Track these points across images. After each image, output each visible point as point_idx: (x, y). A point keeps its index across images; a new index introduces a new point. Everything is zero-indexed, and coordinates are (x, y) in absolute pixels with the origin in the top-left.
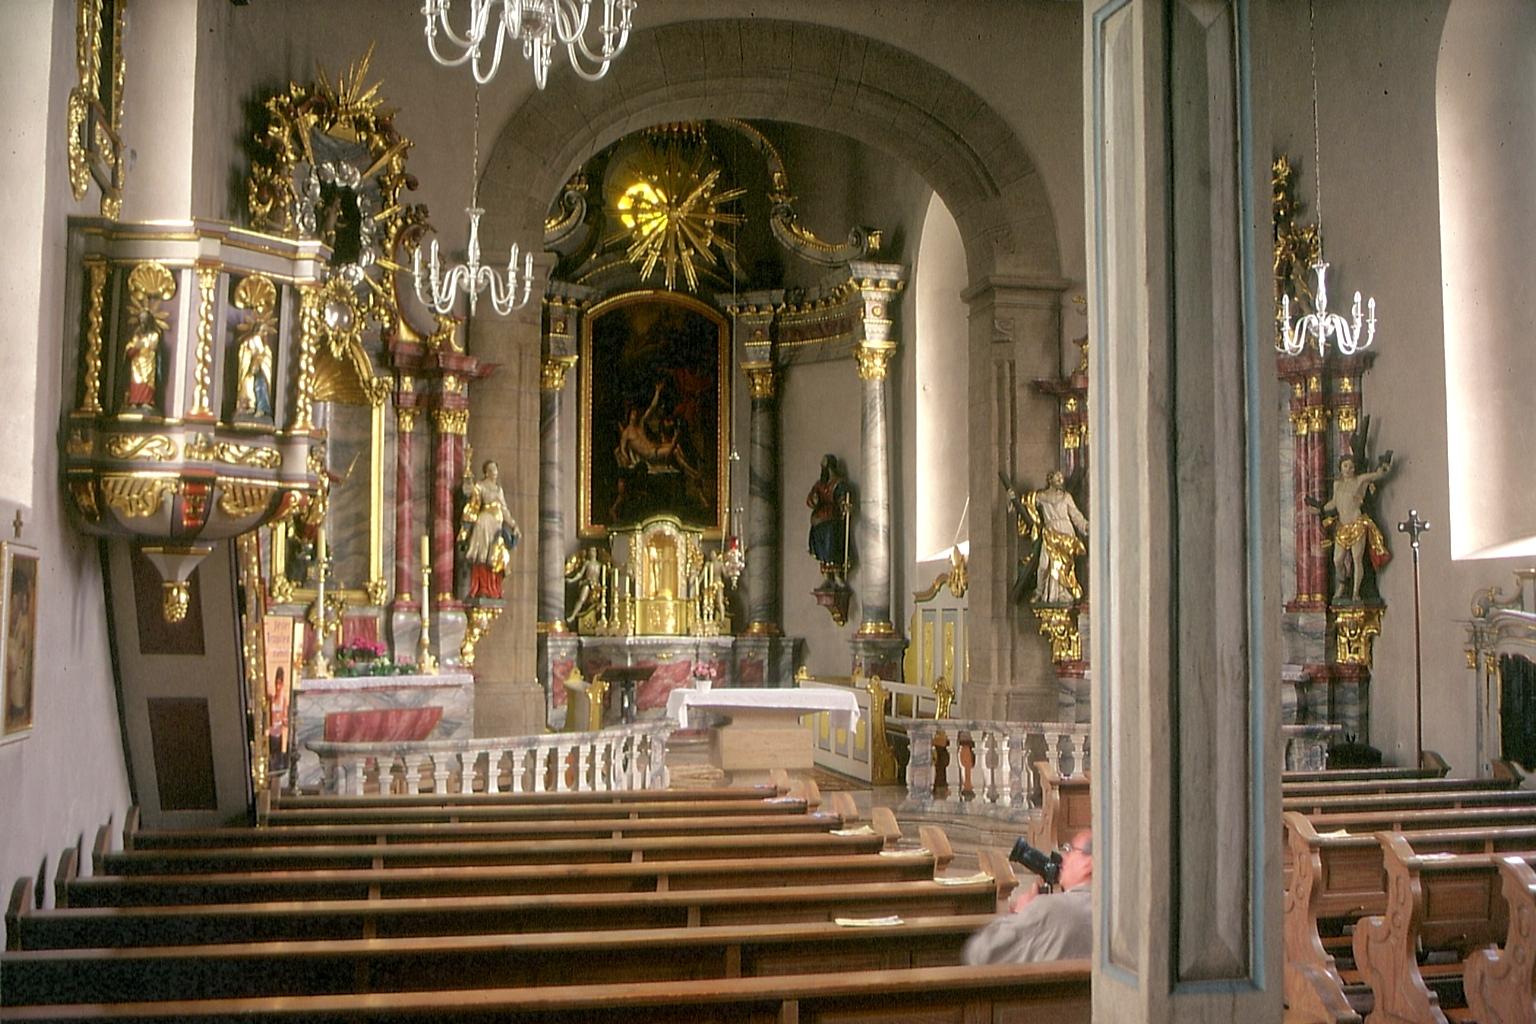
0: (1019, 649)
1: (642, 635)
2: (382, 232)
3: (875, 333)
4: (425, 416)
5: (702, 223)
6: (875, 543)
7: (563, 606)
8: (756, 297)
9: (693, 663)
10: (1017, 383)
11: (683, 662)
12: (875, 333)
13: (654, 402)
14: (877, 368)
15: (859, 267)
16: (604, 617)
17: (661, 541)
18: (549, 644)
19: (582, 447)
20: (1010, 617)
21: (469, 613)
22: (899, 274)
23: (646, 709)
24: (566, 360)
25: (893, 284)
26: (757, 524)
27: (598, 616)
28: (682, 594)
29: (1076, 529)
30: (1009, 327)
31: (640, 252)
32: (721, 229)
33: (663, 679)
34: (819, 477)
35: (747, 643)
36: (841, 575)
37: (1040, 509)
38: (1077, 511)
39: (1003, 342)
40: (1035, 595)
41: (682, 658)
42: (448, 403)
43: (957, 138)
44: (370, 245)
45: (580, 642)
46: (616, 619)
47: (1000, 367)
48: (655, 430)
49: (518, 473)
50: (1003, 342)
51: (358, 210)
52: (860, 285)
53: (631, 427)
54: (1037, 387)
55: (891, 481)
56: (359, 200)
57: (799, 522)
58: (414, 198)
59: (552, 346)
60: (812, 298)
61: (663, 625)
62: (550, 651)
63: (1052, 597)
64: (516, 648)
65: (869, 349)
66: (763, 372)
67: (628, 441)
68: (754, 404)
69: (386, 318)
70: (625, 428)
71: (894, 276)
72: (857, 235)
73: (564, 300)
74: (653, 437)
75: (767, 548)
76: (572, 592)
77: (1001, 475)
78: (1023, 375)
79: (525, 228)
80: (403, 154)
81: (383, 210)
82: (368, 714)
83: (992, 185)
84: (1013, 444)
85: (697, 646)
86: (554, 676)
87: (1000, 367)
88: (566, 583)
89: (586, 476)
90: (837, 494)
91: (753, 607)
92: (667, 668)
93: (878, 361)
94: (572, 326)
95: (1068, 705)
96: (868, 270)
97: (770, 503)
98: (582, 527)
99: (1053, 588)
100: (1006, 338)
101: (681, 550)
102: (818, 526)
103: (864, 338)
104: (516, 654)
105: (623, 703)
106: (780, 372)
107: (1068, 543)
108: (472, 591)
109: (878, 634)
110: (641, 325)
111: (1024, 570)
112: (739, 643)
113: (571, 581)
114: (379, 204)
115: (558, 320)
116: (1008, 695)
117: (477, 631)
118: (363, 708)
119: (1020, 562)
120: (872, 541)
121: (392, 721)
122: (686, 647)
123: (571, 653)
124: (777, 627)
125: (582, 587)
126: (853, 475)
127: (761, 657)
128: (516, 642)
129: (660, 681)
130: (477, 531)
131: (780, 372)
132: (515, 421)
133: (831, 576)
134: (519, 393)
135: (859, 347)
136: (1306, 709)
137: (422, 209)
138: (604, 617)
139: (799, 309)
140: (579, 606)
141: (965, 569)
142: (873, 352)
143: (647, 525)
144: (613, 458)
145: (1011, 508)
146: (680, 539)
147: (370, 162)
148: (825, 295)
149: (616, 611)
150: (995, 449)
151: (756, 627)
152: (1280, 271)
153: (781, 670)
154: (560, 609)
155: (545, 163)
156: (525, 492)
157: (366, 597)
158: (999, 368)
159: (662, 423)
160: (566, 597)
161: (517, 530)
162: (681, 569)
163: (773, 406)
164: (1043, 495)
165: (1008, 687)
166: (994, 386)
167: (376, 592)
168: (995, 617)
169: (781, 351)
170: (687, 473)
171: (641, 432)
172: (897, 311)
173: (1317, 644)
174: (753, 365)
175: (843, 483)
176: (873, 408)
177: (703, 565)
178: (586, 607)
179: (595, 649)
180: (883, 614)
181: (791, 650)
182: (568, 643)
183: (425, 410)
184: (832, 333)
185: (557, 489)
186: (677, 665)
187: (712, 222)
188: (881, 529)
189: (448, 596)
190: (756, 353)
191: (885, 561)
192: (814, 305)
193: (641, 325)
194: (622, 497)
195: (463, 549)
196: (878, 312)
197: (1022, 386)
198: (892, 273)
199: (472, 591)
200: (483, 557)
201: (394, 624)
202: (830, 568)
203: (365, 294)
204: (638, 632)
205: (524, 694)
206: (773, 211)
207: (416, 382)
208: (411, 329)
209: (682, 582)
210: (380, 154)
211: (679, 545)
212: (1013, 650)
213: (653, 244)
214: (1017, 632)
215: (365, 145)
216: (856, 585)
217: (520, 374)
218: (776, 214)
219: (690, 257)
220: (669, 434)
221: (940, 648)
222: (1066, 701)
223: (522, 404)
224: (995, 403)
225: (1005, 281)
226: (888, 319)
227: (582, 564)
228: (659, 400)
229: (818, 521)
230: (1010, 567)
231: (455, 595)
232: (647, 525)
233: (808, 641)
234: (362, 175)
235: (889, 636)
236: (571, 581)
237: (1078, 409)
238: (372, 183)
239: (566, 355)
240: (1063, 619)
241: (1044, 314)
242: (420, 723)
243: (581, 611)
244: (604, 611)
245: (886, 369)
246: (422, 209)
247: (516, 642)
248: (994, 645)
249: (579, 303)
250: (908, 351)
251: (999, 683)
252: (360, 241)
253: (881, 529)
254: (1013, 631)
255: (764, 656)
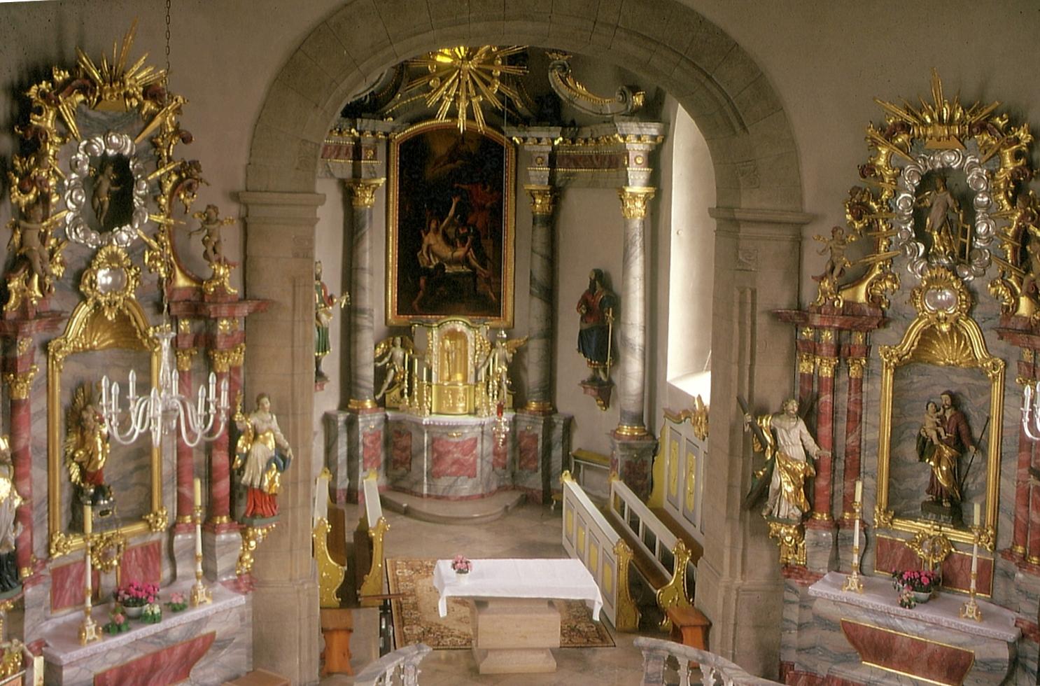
0: (749, 549)
1: (438, 413)
2: (157, 189)
3: (637, 183)
4: (201, 355)
5: (490, 73)
6: (633, 360)
7: (373, 386)
8: (536, 132)
9: (479, 441)
10: (758, 309)
11: (470, 439)
12: (637, 183)
13: (451, 213)
14: (638, 210)
15: (624, 125)
16: (406, 396)
17: (454, 335)
18: (360, 420)
19: (391, 251)
20: (742, 519)
21: (244, 533)
22: (659, 130)
23: (439, 477)
24: (375, 182)
25: (654, 138)
26: (535, 320)
27: (402, 394)
28: (471, 380)
29: (807, 453)
30: (752, 258)
31: (436, 98)
32: (503, 78)
33: (453, 453)
34: (588, 287)
35: (526, 419)
36: (605, 371)
37: (774, 433)
38: (809, 437)
39: (747, 270)
40: (766, 506)
41: (469, 437)
42: (221, 344)
43: (709, 78)
44: (145, 206)
45: (386, 416)
46: (416, 400)
47: (743, 292)
48: (452, 236)
49: (293, 394)
50: (747, 270)
51: (131, 173)
52: (625, 139)
53: (431, 235)
54: (776, 316)
55: (648, 290)
56: (131, 163)
57: (570, 325)
58: (188, 153)
59: (363, 170)
60: (584, 136)
61: (454, 407)
62: (361, 425)
63: (782, 514)
64: (291, 550)
65: (631, 193)
66: (542, 194)
67: (429, 247)
68: (534, 219)
69: (162, 270)
70: (426, 234)
71: (654, 132)
72: (623, 93)
73: (374, 133)
74: (449, 242)
75: (543, 341)
76: (380, 374)
77: (740, 400)
78: (763, 303)
79: (297, 169)
80: (178, 111)
81: (158, 169)
82: (138, 661)
83: (742, 124)
84: (752, 365)
85: (482, 426)
86: (364, 445)
87: (743, 292)
88: (375, 367)
89: (393, 274)
90: (602, 303)
91: (531, 388)
92: (457, 445)
93: (639, 204)
94: (381, 149)
95: (793, 603)
96: (632, 128)
97: (545, 301)
98: (390, 318)
99: (783, 506)
100: (749, 268)
101: (471, 343)
102: (586, 330)
103: (627, 184)
104: (291, 555)
105: (381, 625)
106: (556, 193)
107: (799, 467)
108: (247, 512)
109: (633, 436)
110: (441, 149)
111: (756, 484)
112: (518, 418)
113: (379, 364)
114: (153, 163)
115: (367, 149)
116: (737, 590)
117: (253, 543)
118: (134, 657)
119: (754, 475)
120: (629, 358)
121: (164, 658)
122: (473, 427)
123: (379, 424)
124: (551, 405)
125: (388, 370)
126: (616, 287)
127: (536, 432)
128: (292, 543)
129: (451, 456)
130: (251, 459)
131: (556, 193)
132: (289, 349)
133: (596, 370)
134: (293, 321)
135: (623, 191)
136: (1016, 659)
137: (195, 164)
138: (406, 396)
139: (574, 142)
140: (386, 386)
141: (707, 418)
142: (634, 196)
143: (442, 324)
144: (415, 258)
145: (747, 428)
146: (470, 334)
147: (142, 125)
148: (595, 135)
149: (416, 393)
150: (735, 368)
151: (533, 405)
152: (1016, 236)
153: (554, 442)
154: (370, 389)
155: (317, 106)
156: (299, 412)
157: (148, 526)
158: (742, 293)
159: (457, 230)
160: (375, 379)
161: (290, 451)
162: (470, 358)
163: (550, 221)
164: (778, 420)
165: (738, 581)
166: (736, 310)
167: (157, 522)
168: (729, 518)
169: (558, 175)
170: (478, 272)
171: (440, 238)
172: (656, 160)
173: (1033, 604)
174: (533, 187)
175: (607, 296)
176: (633, 244)
177: (490, 352)
178: (392, 385)
179: (399, 422)
180: (637, 419)
181: (562, 427)
182: (376, 417)
183: (202, 349)
184: (601, 166)
185: (367, 291)
186: (465, 442)
187: (499, 73)
188: (637, 347)
189: (225, 519)
190: (537, 176)
191: (641, 374)
192: (586, 141)
193: (441, 149)
194: (425, 292)
195: (239, 474)
196: (639, 161)
197: (763, 312)
198: (653, 129)
199: (247, 512)
200: (256, 484)
201: (175, 546)
202: (594, 365)
203: (141, 250)
204: (433, 411)
205: (298, 591)
206: (550, 66)
207: (193, 323)
208: (186, 275)
209: (471, 369)
210: (152, 116)
211: (469, 338)
212: (744, 549)
213: (448, 90)
214: (748, 533)
215: (136, 111)
216: (616, 379)
217: (294, 305)
218: (552, 69)
219: (480, 103)
220: (464, 240)
221: (685, 472)
222: (791, 599)
223: (296, 331)
224: (736, 326)
225: (750, 216)
226: (649, 167)
227: (389, 349)
228: (455, 211)
229: (586, 326)
230: (744, 476)
231: (232, 516)
232: (442, 324)
233: (576, 418)
234: (133, 140)
235: (640, 438)
236: (379, 364)
237: (814, 337)
238: (146, 144)
239: (375, 178)
240: (791, 531)
241: (786, 245)
242: (193, 650)
243: (388, 389)
244: (406, 391)
245: (645, 210)
246: (195, 164)
247: (292, 543)
248: (727, 542)
249: (386, 134)
250: (664, 195)
251: (731, 576)
252: (134, 203)
253: (637, 347)
254: (744, 534)
255: (539, 431)
